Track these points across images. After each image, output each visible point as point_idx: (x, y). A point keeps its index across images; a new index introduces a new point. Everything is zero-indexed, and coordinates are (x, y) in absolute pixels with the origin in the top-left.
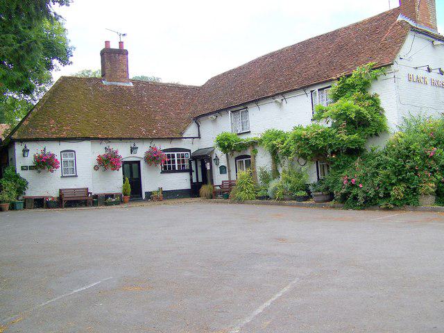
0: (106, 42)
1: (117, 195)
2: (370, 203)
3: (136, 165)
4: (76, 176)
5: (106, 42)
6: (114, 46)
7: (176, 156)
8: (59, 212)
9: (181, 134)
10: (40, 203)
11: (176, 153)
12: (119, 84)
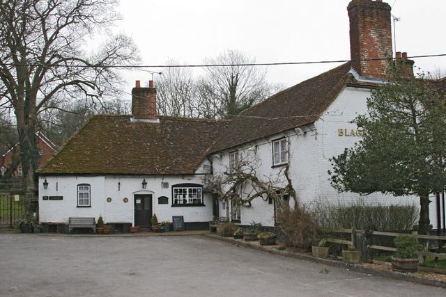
0: (137, 81)
1: (268, 229)
2: (108, 233)
3: (148, 198)
4: (90, 206)
5: (137, 81)
6: (144, 85)
7: (187, 191)
8: (115, 240)
9: (194, 170)
10: (53, 228)
11: (188, 188)
12: (149, 121)
